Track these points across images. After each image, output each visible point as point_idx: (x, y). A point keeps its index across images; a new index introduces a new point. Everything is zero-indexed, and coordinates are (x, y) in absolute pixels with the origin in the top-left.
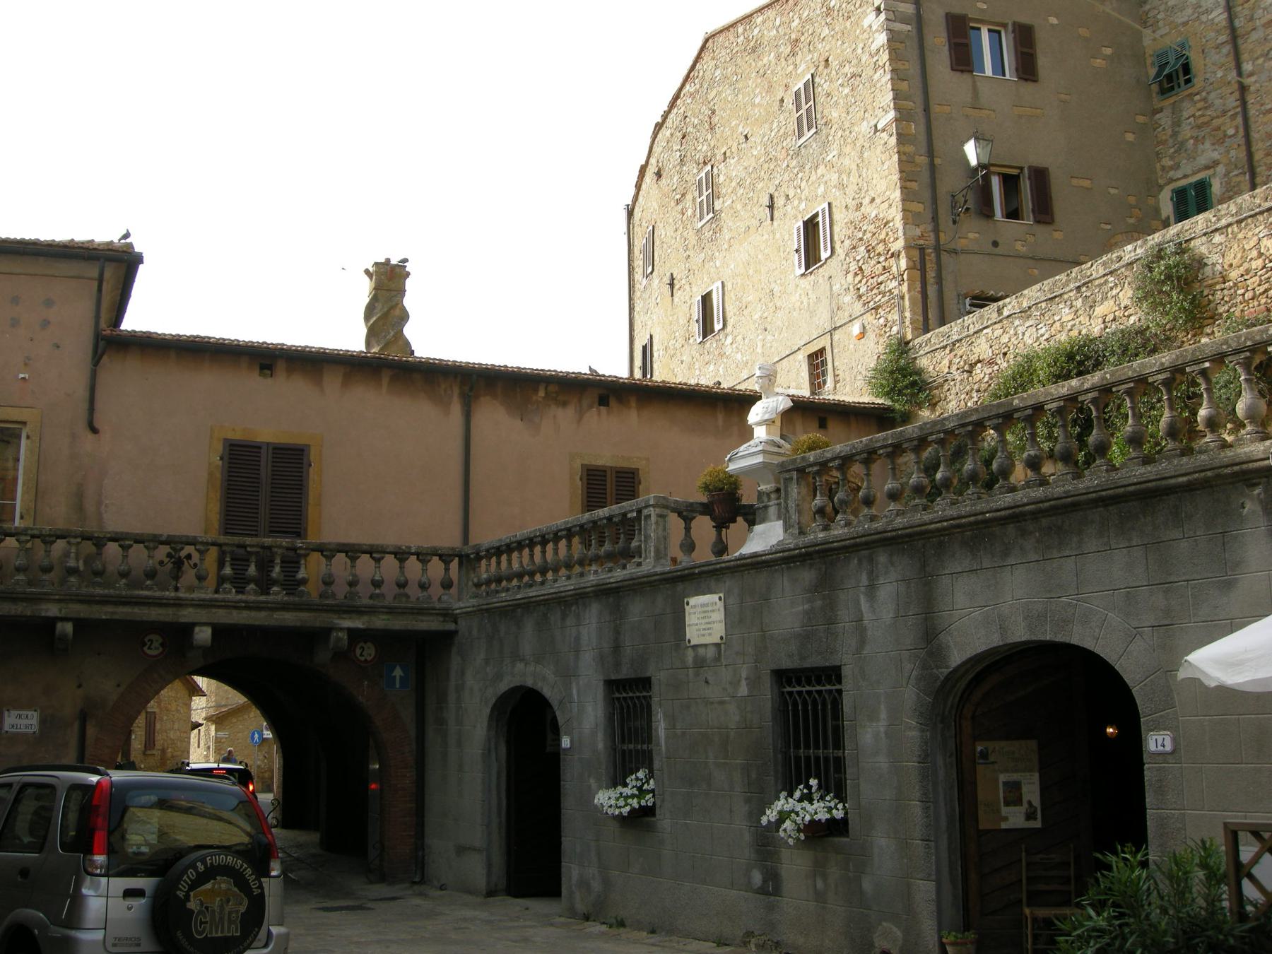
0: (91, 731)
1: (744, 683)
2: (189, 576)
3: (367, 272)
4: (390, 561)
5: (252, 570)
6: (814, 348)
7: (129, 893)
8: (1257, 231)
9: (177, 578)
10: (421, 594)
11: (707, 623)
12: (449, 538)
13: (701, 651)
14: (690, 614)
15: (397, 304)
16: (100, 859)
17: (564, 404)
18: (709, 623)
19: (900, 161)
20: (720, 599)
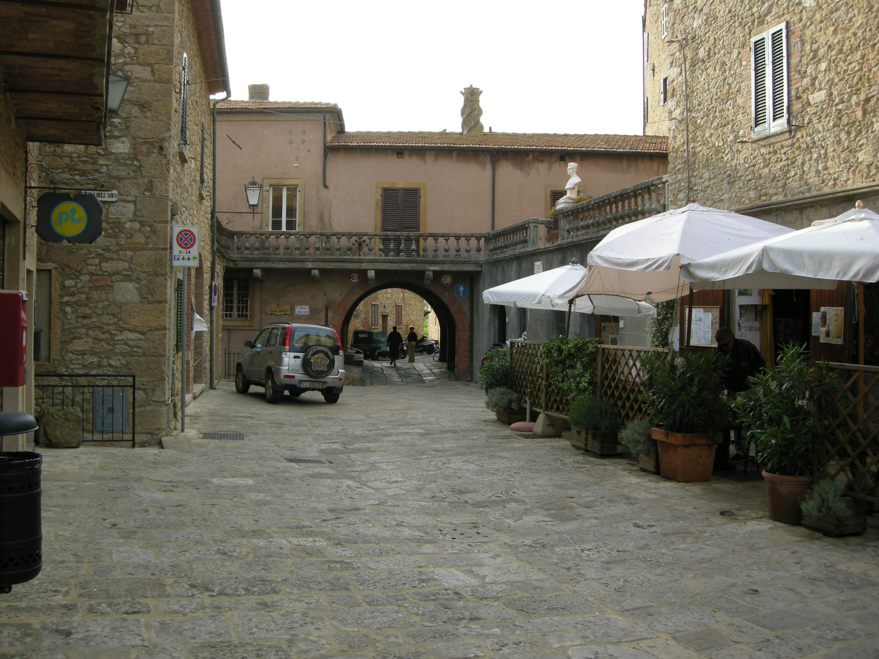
0: (330, 314)
2: (365, 249)
3: (461, 92)
4: (452, 241)
5: (392, 246)
7: (295, 357)
9: (360, 250)
10: (466, 254)
12: (485, 228)
15: (475, 108)
16: (287, 347)
17: (542, 161)
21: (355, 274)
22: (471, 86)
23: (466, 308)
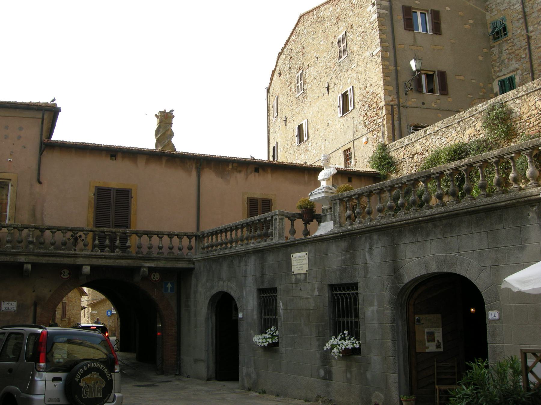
0: (39, 310)
1: (316, 290)
2: (80, 245)
3: (156, 115)
4: (166, 238)
5: (107, 242)
6: (346, 148)
7: (55, 379)
8: (535, 98)
9: (75, 245)
10: (179, 252)
11: (301, 265)
12: (191, 229)
13: (298, 276)
14: (293, 261)
15: (169, 129)
16: (42, 365)
17: (240, 172)
18: (302, 265)
19: (383, 68)
20: (306, 254)
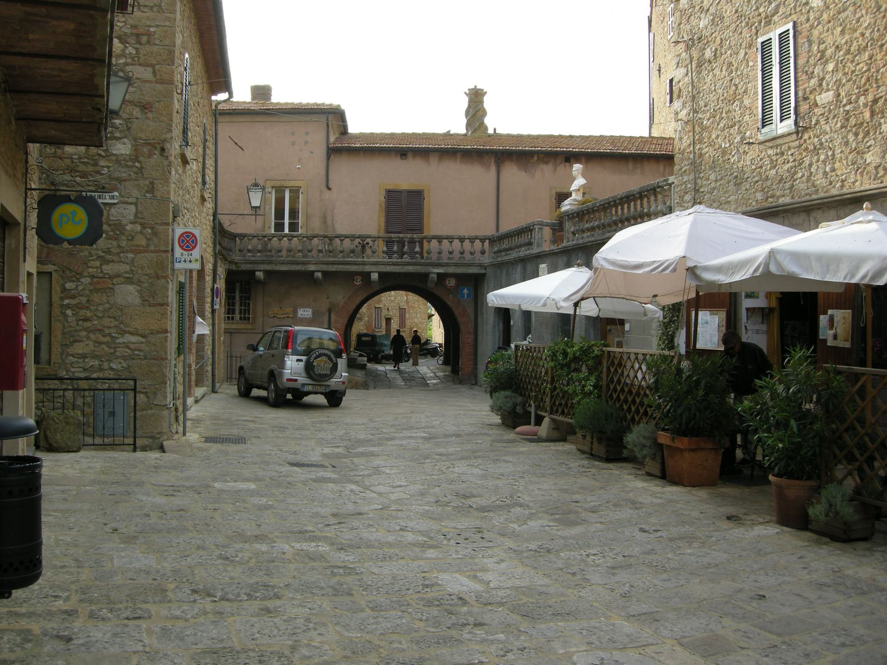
0: (333, 317)
2: (368, 251)
3: (465, 93)
4: (456, 243)
5: (395, 248)
7: (298, 360)
9: (363, 252)
10: (470, 257)
12: (489, 230)
15: (480, 109)
16: (290, 350)
17: (547, 163)
21: (358, 277)
22: (476, 86)
23: (470, 311)
